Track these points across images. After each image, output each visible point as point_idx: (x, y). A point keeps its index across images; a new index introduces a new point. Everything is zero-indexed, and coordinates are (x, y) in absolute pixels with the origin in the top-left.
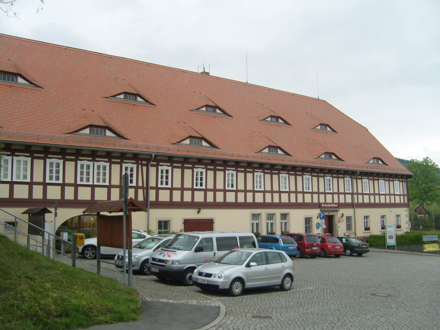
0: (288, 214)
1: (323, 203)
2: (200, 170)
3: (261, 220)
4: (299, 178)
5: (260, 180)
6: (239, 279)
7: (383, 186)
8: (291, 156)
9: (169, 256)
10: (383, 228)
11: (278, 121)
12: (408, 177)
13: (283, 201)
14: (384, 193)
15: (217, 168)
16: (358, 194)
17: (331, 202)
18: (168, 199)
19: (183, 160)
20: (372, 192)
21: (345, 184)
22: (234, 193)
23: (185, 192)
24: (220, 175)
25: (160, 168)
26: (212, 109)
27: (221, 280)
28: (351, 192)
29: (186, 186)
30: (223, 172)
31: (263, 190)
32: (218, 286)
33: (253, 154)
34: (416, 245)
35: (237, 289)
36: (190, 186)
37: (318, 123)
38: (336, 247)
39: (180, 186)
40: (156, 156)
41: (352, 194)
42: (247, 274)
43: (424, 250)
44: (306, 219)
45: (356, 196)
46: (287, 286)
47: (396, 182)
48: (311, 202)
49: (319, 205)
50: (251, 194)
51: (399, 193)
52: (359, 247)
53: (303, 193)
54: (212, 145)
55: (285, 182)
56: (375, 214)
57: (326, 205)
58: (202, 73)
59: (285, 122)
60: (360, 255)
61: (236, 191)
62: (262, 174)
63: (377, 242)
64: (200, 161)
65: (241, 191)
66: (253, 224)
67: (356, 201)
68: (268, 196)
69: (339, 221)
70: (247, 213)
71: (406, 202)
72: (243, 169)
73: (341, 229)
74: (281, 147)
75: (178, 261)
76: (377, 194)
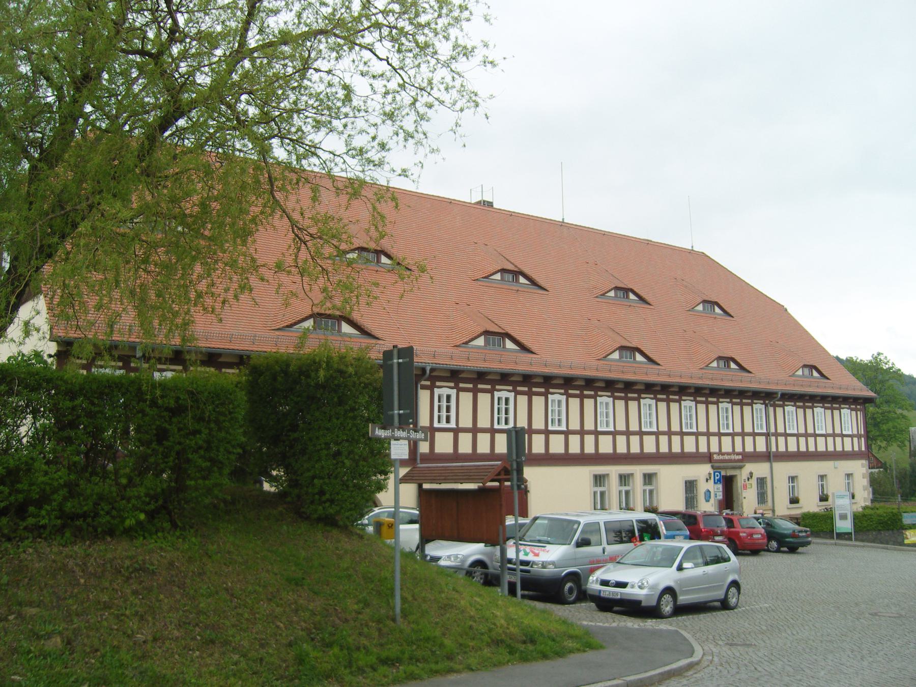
0: (655, 474)
1: (715, 453)
2: (504, 395)
3: (609, 485)
4: (589, 403)
5: (607, 411)
6: (669, 590)
7: (820, 418)
8: (750, 372)
9: (537, 555)
10: (824, 498)
11: (628, 297)
12: (867, 400)
13: (552, 450)
14: (824, 432)
15: (534, 389)
16: (777, 435)
17: (730, 450)
18: (450, 450)
19: (475, 376)
20: (802, 431)
21: (755, 416)
22: (451, 435)
23: (480, 436)
24: (538, 402)
25: (437, 391)
26: (511, 276)
27: (644, 592)
28: (764, 431)
29: (480, 425)
30: (543, 398)
31: (454, 426)
32: (639, 602)
33: (595, 363)
34: (890, 532)
35: (667, 608)
36: (543, 427)
37: (700, 300)
38: (755, 536)
39: (470, 426)
40: (432, 370)
41: (767, 435)
42: (681, 582)
43: (906, 542)
44: (686, 482)
45: (773, 439)
46: (733, 601)
47: (845, 412)
48: (694, 450)
49: (708, 458)
50: (488, 436)
51: (850, 433)
52: (793, 535)
53: (596, 433)
54: (523, 348)
55: (650, 413)
56: (807, 471)
57: (721, 457)
58: (479, 203)
59: (533, 282)
60: (793, 549)
61: (456, 431)
62: (563, 398)
63: (820, 525)
64: (505, 378)
65: (465, 430)
66: (595, 493)
67: (774, 449)
68: (574, 440)
69: (745, 487)
70: (585, 473)
71: (863, 449)
72: (471, 386)
73: (748, 501)
74: (512, 334)
75: (553, 563)
76: (838, 435)
